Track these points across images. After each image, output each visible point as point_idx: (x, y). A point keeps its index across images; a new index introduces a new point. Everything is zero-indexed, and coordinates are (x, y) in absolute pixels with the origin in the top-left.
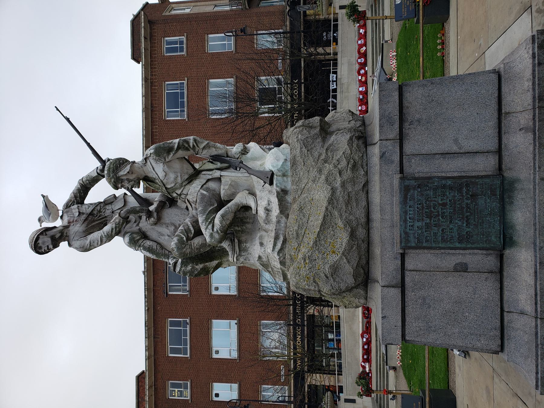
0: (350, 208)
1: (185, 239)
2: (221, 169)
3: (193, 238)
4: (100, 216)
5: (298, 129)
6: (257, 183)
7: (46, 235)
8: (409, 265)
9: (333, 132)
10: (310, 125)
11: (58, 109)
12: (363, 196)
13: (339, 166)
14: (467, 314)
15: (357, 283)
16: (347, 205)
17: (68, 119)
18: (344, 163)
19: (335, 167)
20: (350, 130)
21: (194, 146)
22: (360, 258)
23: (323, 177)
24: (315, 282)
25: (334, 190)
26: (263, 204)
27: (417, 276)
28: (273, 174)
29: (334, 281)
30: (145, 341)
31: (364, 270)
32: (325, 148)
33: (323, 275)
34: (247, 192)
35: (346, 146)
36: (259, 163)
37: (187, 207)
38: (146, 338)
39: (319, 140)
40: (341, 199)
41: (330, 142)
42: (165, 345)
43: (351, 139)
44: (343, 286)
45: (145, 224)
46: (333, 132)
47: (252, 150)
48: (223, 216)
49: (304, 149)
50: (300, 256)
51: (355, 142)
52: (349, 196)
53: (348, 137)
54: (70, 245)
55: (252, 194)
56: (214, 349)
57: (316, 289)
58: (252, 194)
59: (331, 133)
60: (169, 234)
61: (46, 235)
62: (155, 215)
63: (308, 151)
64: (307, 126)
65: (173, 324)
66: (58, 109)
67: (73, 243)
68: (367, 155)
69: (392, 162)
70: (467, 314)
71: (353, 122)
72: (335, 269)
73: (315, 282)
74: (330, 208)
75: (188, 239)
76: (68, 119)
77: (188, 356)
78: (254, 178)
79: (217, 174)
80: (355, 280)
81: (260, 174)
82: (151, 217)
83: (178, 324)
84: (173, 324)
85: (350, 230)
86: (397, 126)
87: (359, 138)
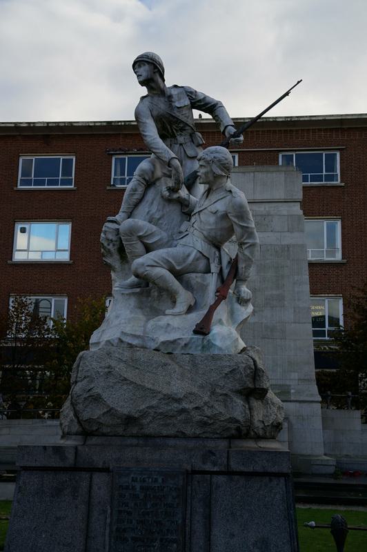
0: (159, 417)
1: (141, 234)
2: (221, 272)
3: (142, 242)
4: (175, 130)
5: (252, 363)
6: (196, 317)
7: (154, 73)
8: (99, 479)
9: (249, 403)
10: (258, 378)
11: (299, 82)
12: (172, 431)
13: (206, 408)
14: (44, 536)
15: (82, 423)
16: (161, 414)
17: (287, 94)
18: (208, 412)
19: (206, 403)
20: (250, 421)
21: (246, 243)
22: (107, 426)
23: (195, 390)
24: (85, 377)
25: (178, 401)
26: (175, 322)
27: (85, 484)
28: (120, 339)
29: (85, 399)
30: (44, 123)
31: (97, 430)
32: (229, 393)
33: (92, 386)
34: (192, 304)
35: (228, 416)
36: (224, 317)
37: (182, 232)
38: (48, 123)
39: (238, 387)
40: (169, 408)
41: (235, 399)
42: (33, 151)
43: (237, 421)
44: (80, 407)
45: (163, 186)
46: (249, 403)
47: (243, 309)
48: (162, 277)
49: (228, 370)
50: (113, 363)
51: (233, 426)
52: (171, 416)
53: (240, 418)
54: (143, 98)
55: (190, 309)
56: (26, 226)
57: (78, 379)
58: (190, 309)
59: (247, 400)
60: (151, 213)
61: (154, 73)
62: (175, 196)
63: (226, 374)
64: (255, 374)
65: (67, 163)
66: (299, 82)
67: (146, 101)
68: (218, 438)
69: (204, 463)
70: (44, 536)
71: (261, 426)
72: (97, 399)
73: (85, 377)
74: (160, 396)
75: (140, 238)
76: (287, 94)
77: (19, 187)
78: (205, 312)
79: (214, 268)
80: (86, 420)
81: (207, 319)
82: (169, 192)
83: (67, 171)
84: (67, 163)
85: (136, 416)
86: (242, 468)
87: (238, 429)
